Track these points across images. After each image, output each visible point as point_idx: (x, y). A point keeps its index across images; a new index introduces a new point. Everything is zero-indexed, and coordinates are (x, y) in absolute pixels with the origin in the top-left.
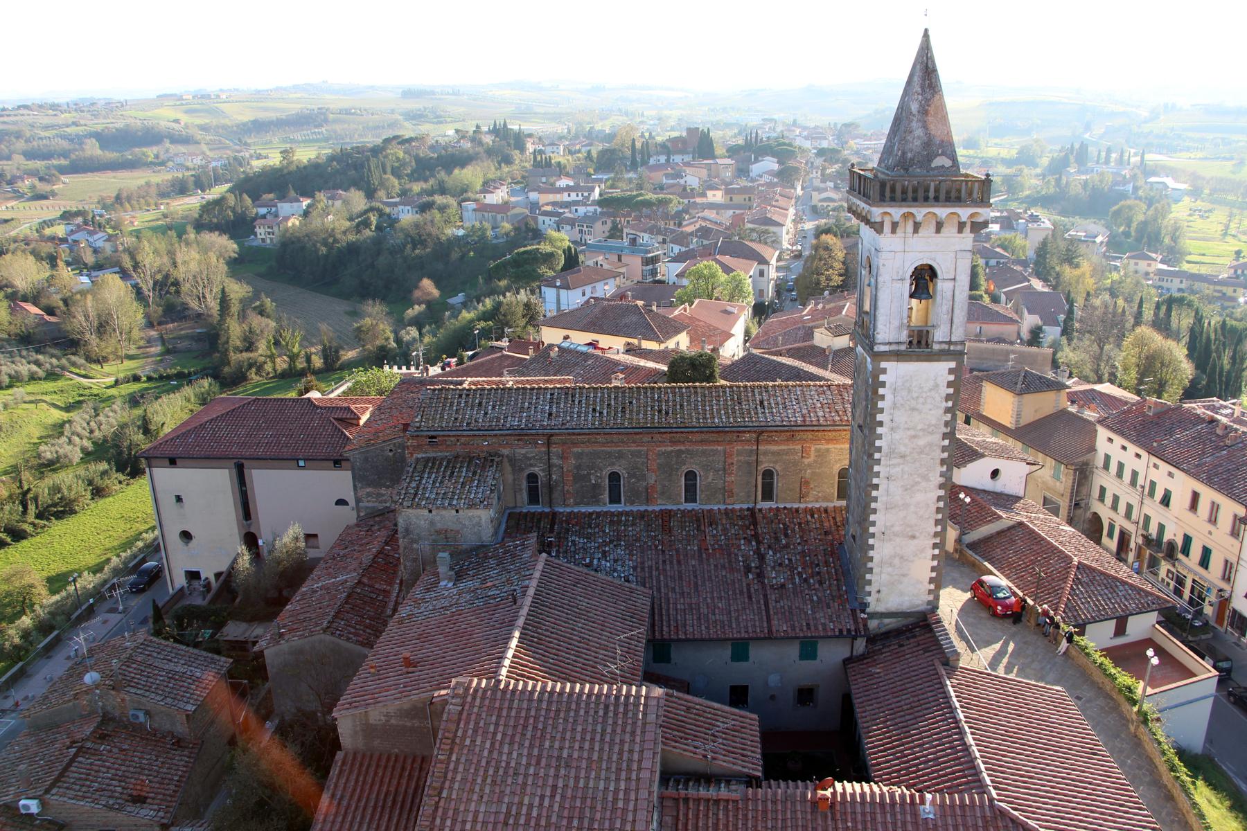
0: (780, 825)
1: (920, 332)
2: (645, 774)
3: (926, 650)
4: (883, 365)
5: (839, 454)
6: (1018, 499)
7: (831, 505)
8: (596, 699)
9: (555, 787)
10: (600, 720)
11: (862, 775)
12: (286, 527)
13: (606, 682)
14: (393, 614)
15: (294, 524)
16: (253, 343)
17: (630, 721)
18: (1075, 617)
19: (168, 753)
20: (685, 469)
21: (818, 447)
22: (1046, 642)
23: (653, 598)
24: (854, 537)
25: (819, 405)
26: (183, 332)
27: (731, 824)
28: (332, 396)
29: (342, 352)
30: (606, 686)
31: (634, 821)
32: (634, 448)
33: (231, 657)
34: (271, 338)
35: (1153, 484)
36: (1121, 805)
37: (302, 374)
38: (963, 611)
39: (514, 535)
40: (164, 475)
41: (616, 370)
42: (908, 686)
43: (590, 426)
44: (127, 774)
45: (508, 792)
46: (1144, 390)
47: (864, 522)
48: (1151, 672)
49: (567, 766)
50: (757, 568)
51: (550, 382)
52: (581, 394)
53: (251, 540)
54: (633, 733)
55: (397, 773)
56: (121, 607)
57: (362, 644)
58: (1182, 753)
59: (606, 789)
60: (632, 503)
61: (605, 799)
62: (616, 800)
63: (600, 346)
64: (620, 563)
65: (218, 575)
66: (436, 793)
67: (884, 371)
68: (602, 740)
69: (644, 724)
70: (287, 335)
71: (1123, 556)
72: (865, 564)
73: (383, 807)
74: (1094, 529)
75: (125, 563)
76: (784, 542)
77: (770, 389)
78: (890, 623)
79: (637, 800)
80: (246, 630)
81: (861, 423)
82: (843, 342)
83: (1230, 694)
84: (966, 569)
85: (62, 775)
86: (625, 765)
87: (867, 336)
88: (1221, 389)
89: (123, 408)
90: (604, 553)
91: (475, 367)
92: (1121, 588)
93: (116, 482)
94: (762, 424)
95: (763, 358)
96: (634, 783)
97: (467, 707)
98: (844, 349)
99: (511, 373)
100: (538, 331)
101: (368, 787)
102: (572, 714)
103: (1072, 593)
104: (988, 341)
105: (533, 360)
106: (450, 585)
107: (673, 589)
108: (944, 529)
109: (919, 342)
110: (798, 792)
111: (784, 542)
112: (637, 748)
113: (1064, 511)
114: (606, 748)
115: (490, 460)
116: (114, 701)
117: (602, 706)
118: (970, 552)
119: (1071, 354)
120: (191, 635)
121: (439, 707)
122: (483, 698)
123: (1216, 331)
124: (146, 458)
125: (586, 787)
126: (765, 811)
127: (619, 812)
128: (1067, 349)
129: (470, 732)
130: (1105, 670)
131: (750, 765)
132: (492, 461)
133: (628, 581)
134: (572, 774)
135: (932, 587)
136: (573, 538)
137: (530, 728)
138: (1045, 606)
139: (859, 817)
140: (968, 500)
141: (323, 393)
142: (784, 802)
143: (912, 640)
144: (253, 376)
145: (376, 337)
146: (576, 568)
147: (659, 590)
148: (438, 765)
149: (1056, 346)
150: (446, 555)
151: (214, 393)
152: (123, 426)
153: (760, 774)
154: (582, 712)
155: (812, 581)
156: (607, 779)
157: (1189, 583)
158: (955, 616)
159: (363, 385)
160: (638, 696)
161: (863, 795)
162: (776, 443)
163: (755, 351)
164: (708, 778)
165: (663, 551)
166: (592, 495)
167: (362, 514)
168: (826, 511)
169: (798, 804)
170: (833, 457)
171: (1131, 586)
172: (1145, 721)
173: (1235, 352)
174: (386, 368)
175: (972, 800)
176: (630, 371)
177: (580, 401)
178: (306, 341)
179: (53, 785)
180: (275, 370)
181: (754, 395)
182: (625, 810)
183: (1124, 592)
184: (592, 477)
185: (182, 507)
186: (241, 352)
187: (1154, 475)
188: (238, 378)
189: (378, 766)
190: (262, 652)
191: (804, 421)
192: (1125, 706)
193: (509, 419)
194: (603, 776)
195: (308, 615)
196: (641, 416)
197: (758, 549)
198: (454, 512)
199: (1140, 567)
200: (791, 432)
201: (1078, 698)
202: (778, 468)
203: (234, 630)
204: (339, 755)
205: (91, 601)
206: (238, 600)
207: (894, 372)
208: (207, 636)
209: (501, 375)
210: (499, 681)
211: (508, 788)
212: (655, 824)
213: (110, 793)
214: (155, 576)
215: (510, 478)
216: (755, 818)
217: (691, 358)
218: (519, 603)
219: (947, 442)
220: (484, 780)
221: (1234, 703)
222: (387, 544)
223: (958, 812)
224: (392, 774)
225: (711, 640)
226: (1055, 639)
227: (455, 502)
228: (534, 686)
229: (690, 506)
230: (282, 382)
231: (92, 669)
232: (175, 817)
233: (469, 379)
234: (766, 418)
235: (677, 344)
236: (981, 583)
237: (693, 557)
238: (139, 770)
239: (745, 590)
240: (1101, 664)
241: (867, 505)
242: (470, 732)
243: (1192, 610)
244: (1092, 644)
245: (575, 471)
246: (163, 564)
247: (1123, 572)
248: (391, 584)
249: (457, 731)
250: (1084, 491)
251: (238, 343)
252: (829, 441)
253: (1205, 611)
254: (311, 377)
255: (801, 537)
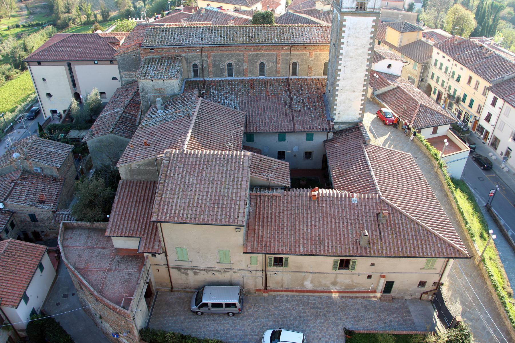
0: (297, 206)
1: (362, 3)
2: (244, 186)
3: (357, 138)
4: (345, 17)
5: (324, 56)
6: (398, 77)
7: (320, 77)
8: (224, 157)
9: (208, 192)
10: (225, 165)
11: (329, 186)
12: (92, 90)
13: (228, 150)
14: (139, 124)
15: (95, 88)
16: (70, 9)
17: (237, 165)
18: (417, 126)
19: (51, 184)
20: (260, 62)
21: (316, 53)
22: (405, 135)
23: (246, 116)
24: (329, 91)
25: (317, 35)
26: (36, 4)
27: (278, 205)
28: (107, 32)
29: (110, 13)
30: (227, 152)
31: (239, 204)
32: (238, 53)
33: (73, 145)
34: (78, 7)
35: (454, 73)
36: (428, 198)
37: (93, 23)
38: (373, 122)
39: (188, 90)
40: (36, 69)
41: (230, 19)
42: (349, 152)
43: (219, 43)
44: (36, 192)
45: (189, 194)
46: (455, 32)
47: (334, 84)
48: (445, 148)
49: (212, 183)
50: (289, 103)
51: (202, 24)
52: (215, 29)
53: (77, 96)
54: (239, 170)
55: (144, 188)
56: (25, 126)
57: (127, 137)
58: (453, 179)
59: (228, 192)
60: (237, 76)
61: (228, 196)
62: (232, 196)
63: (223, 8)
64: (232, 101)
65: (64, 111)
66: (160, 195)
67: (345, 20)
68: (226, 173)
69: (243, 166)
70: (85, 5)
71: (439, 102)
72: (334, 102)
73: (140, 202)
74: (428, 91)
75: (24, 108)
76: (301, 92)
77: (296, 27)
78: (343, 126)
79: (240, 196)
80: (79, 133)
81: (335, 43)
82: (328, 8)
83: (474, 157)
84: (375, 105)
85: (10, 193)
86: (235, 182)
87: (339, 5)
88: (487, 33)
89: (13, 40)
90: (226, 97)
91: (169, 18)
92: (437, 115)
93: (15, 73)
94: (293, 43)
95: (294, 14)
96: (239, 190)
97: (171, 161)
98: (328, 11)
99: (184, 20)
100: (196, 2)
101: (133, 194)
102: (214, 163)
103: (417, 116)
104: (390, 9)
105: (194, 15)
106: (162, 111)
107: (255, 112)
108: (367, 88)
109: (361, 8)
110: (304, 193)
111: (301, 92)
112: (240, 176)
113: (416, 83)
114: (228, 176)
115: (176, 58)
116: (27, 164)
117: (226, 159)
118: (377, 98)
119: (425, 16)
120: (56, 136)
121: (160, 161)
122: (177, 157)
123: (488, 7)
124: (27, 62)
125: (220, 191)
126: (291, 200)
127: (233, 201)
128: (424, 14)
129: (173, 171)
130: (427, 147)
131: (286, 182)
132: (178, 59)
133: (236, 109)
134: (215, 187)
135: (361, 112)
136: (213, 91)
137: (197, 169)
138: (406, 121)
139: (328, 202)
140: (377, 77)
141: (103, 31)
142: (299, 197)
143: (352, 133)
144: (71, 24)
145: (125, 6)
146: (215, 104)
147: (249, 112)
148: (161, 184)
149: (419, 12)
150: (160, 99)
151: (54, 32)
152: (15, 48)
153: (289, 186)
154: (218, 162)
155: (312, 109)
156: (228, 188)
157: (463, 114)
158: (370, 124)
159: (120, 27)
160: (240, 156)
161: (330, 194)
162: (298, 51)
163: (290, 11)
164: (269, 188)
165: (250, 96)
166: (221, 73)
167: (123, 83)
168: (318, 80)
169: (304, 197)
170: (322, 57)
171: (441, 114)
172: (441, 167)
173: (495, 16)
174: (130, 19)
175: (372, 196)
176: (236, 19)
177: (214, 33)
178: (94, 8)
179: (7, 197)
180: (81, 22)
181: (289, 30)
182: (236, 200)
183: (437, 117)
184: (221, 65)
185: (46, 83)
186: (65, 13)
187: (455, 69)
188: (64, 26)
189: (136, 186)
190: (86, 142)
191: (310, 41)
192: (434, 161)
193: (184, 40)
194: (227, 187)
195: (104, 126)
196: (241, 39)
197: (290, 95)
198: (162, 81)
199: (445, 106)
200: (304, 46)
201: (416, 158)
202: (299, 61)
203: (73, 134)
204: (121, 182)
205: (12, 124)
206: (74, 121)
207: (350, 21)
208: (62, 136)
209: (180, 22)
210: (184, 150)
211: (189, 193)
212: (248, 205)
213: (30, 200)
214: (38, 113)
215: (185, 66)
216: (287, 203)
217: (262, 14)
218: (191, 118)
219: (370, 52)
220: (179, 190)
221: (475, 161)
222: (135, 95)
223: (366, 200)
224: (142, 188)
225: (270, 133)
226: (409, 135)
227: (162, 77)
228: (198, 152)
229: (262, 77)
230: (85, 27)
231: (16, 152)
232: (57, 208)
233: (167, 24)
234: (294, 40)
235: (257, 8)
236: (381, 111)
237: (263, 99)
238: (41, 191)
239: (284, 112)
240: (426, 145)
241: (335, 78)
242: (173, 171)
243: (463, 124)
244: (423, 137)
245: (213, 63)
246: (40, 108)
247: (438, 108)
248: (137, 112)
249: (167, 171)
250: (425, 74)
251: (63, 9)
252: (320, 50)
253: (468, 125)
254: (97, 24)
255: (308, 91)
